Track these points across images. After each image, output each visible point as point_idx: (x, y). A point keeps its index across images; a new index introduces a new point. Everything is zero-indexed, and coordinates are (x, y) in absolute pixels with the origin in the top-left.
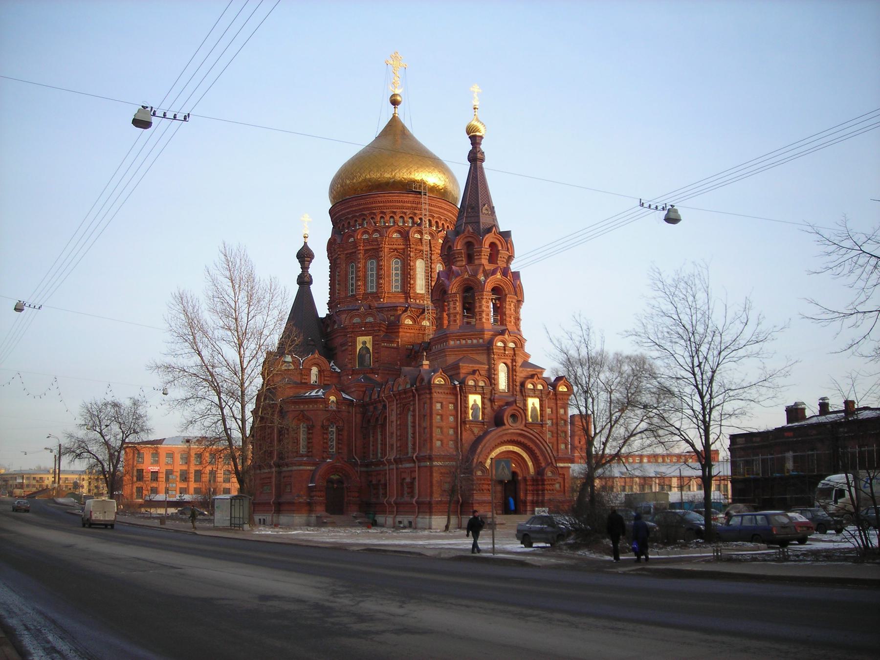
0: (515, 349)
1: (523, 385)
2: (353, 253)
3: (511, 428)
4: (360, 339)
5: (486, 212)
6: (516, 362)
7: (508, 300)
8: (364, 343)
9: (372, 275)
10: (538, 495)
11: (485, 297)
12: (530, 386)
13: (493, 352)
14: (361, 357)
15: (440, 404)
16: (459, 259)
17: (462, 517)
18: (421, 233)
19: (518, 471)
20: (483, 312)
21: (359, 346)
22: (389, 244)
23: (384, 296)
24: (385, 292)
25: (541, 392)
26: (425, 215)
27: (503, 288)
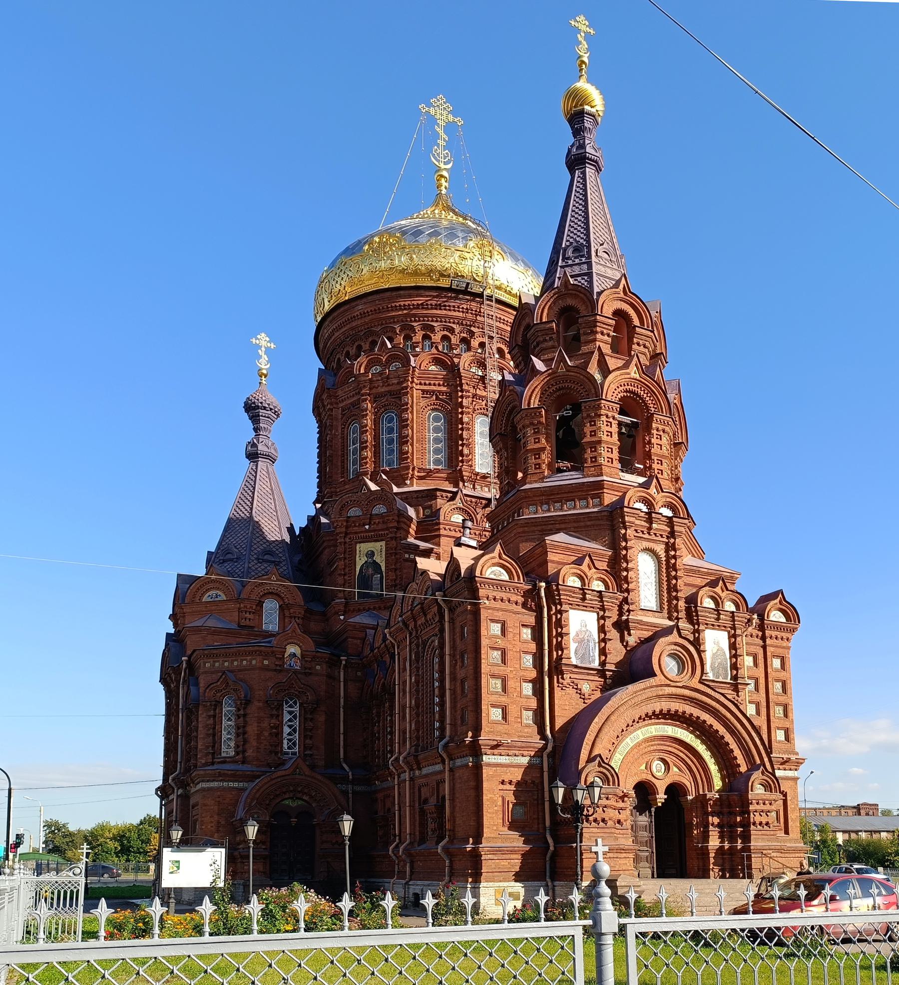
0: (675, 519)
1: (692, 600)
2: (353, 404)
3: (669, 682)
4: (363, 548)
5: (606, 256)
6: (675, 550)
7: (654, 425)
8: (371, 554)
9: (390, 441)
10: (732, 840)
11: (603, 412)
12: (709, 603)
13: (624, 522)
14: (365, 581)
15: (499, 625)
16: (544, 345)
17: (556, 883)
18: (482, 365)
19: (687, 781)
20: (600, 442)
21: (360, 561)
22: (421, 384)
23: (412, 475)
24: (413, 469)
25: (733, 617)
26: (491, 338)
27: (644, 401)
